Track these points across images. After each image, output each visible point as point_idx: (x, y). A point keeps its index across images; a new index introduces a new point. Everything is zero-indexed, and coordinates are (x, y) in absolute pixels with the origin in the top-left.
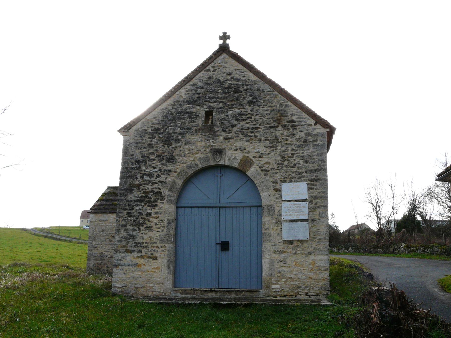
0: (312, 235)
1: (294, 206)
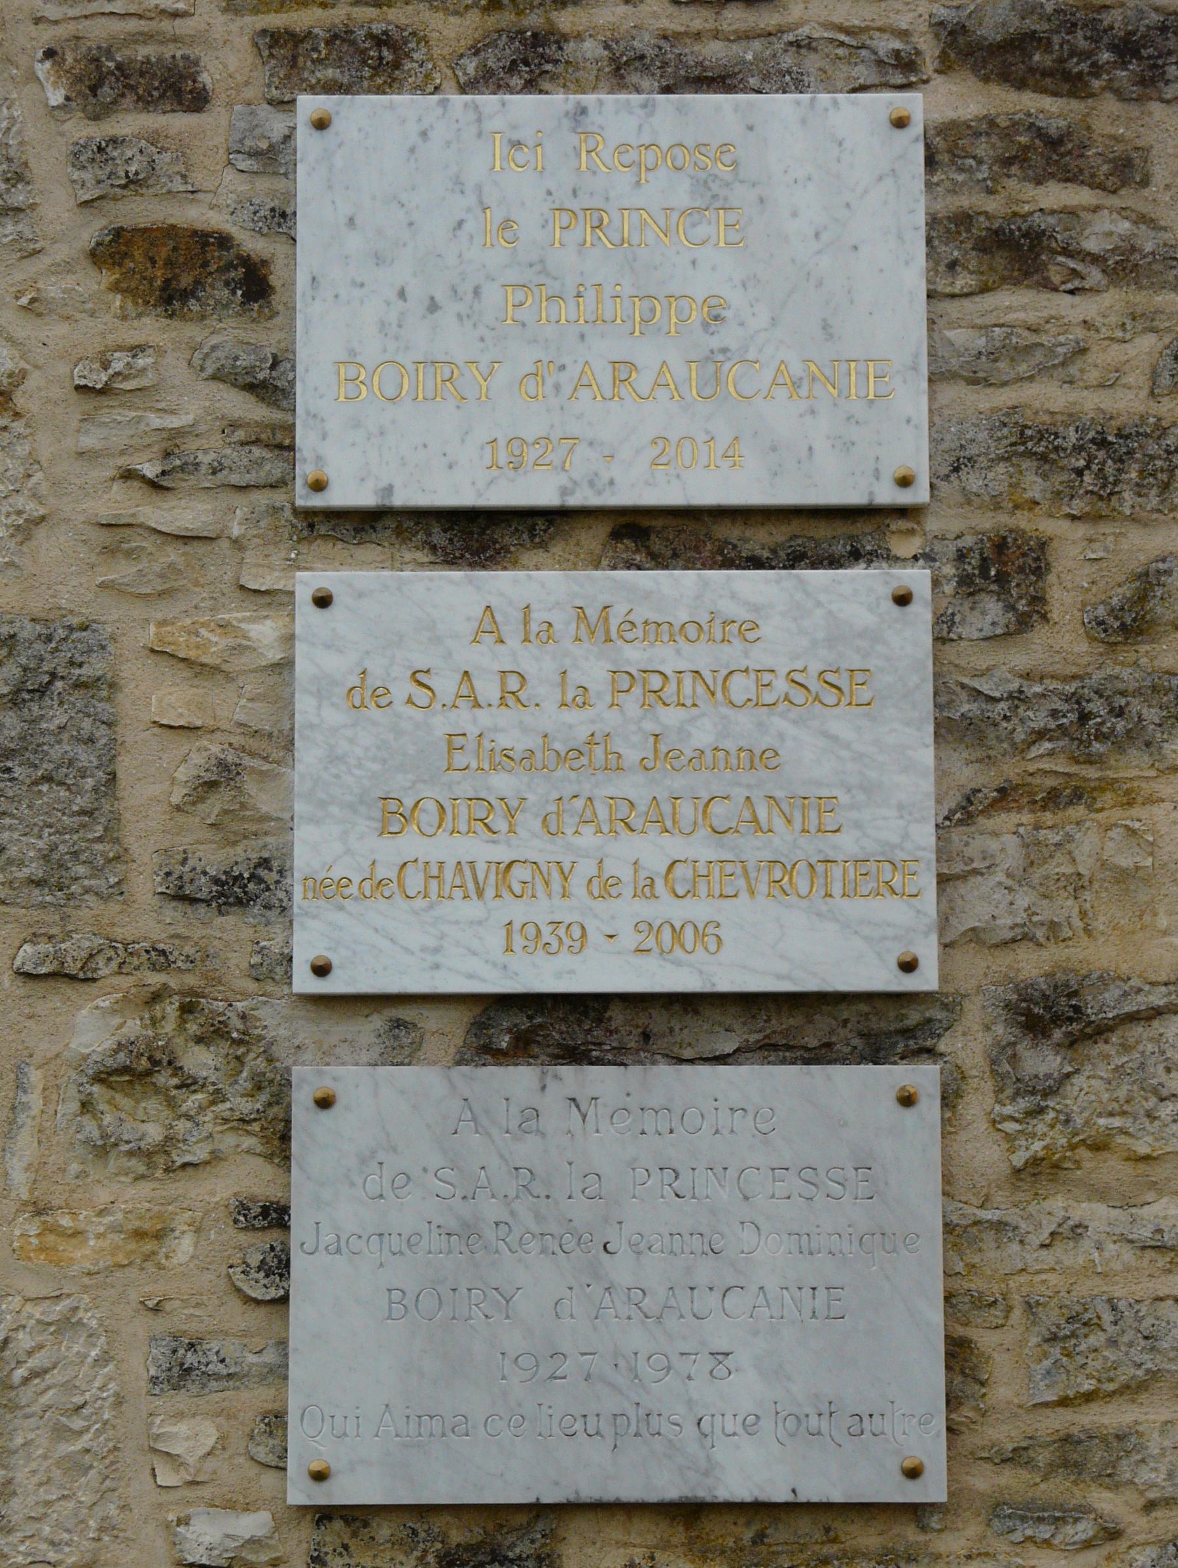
0: (1015, 1375)
1: (593, 670)
